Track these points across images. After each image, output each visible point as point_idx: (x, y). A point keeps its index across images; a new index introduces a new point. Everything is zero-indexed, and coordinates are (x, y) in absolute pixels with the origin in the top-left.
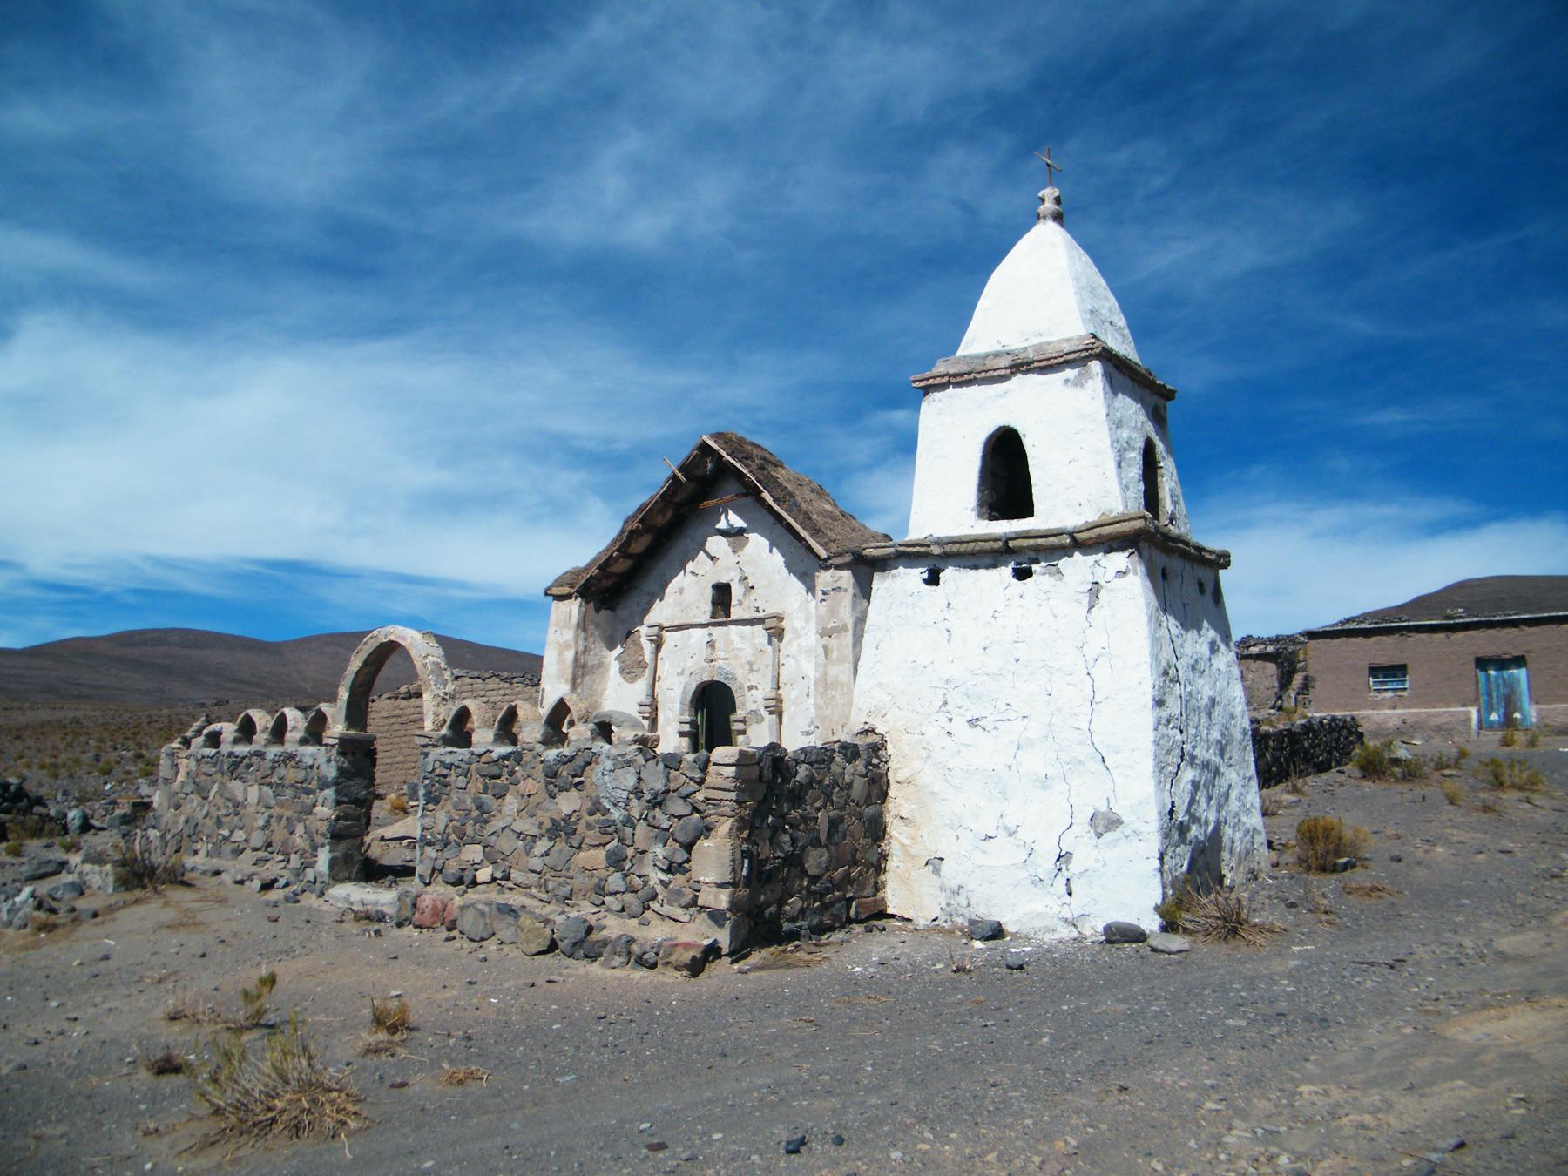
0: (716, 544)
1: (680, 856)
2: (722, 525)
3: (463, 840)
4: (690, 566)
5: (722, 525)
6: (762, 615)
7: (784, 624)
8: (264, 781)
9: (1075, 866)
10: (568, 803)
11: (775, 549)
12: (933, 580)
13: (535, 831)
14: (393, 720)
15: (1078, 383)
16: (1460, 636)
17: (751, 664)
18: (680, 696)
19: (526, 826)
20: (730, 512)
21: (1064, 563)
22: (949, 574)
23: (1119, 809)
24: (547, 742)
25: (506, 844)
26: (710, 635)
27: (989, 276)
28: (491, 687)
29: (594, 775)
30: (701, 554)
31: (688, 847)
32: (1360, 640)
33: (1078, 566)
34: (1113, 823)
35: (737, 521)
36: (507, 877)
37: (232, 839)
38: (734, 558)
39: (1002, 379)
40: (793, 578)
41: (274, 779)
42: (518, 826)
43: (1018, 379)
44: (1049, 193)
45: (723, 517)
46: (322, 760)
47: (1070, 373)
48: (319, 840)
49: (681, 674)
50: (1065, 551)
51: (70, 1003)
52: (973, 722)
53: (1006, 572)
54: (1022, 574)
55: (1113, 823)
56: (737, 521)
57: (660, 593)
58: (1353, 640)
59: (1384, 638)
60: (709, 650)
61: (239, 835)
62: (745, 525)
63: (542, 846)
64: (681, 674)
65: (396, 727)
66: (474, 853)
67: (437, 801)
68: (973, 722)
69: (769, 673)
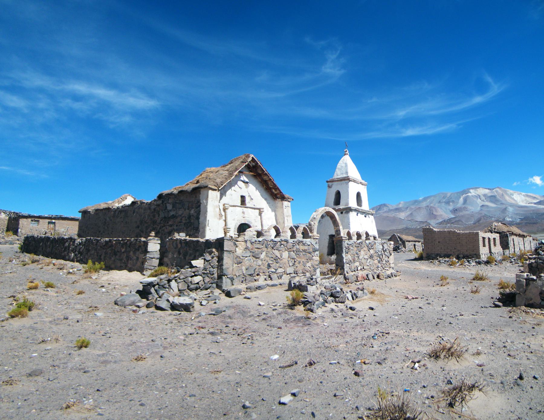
3: (354, 261)
4: (233, 188)
5: (242, 179)
6: (255, 207)
8: (289, 250)
10: (372, 251)
11: (257, 190)
13: (367, 258)
17: (255, 220)
18: (234, 226)
19: (366, 257)
20: (244, 176)
24: (291, 238)
25: (363, 261)
26: (243, 210)
29: (375, 246)
30: (236, 185)
36: (363, 268)
37: (277, 272)
38: (246, 190)
39: (358, 184)
40: (263, 200)
41: (295, 249)
43: (360, 185)
45: (242, 176)
46: (314, 243)
48: (316, 267)
49: (234, 220)
51: (133, 391)
53: (364, 216)
56: (247, 180)
60: (243, 214)
61: (280, 270)
62: (248, 181)
63: (369, 260)
64: (234, 220)
66: (357, 264)
67: (347, 253)
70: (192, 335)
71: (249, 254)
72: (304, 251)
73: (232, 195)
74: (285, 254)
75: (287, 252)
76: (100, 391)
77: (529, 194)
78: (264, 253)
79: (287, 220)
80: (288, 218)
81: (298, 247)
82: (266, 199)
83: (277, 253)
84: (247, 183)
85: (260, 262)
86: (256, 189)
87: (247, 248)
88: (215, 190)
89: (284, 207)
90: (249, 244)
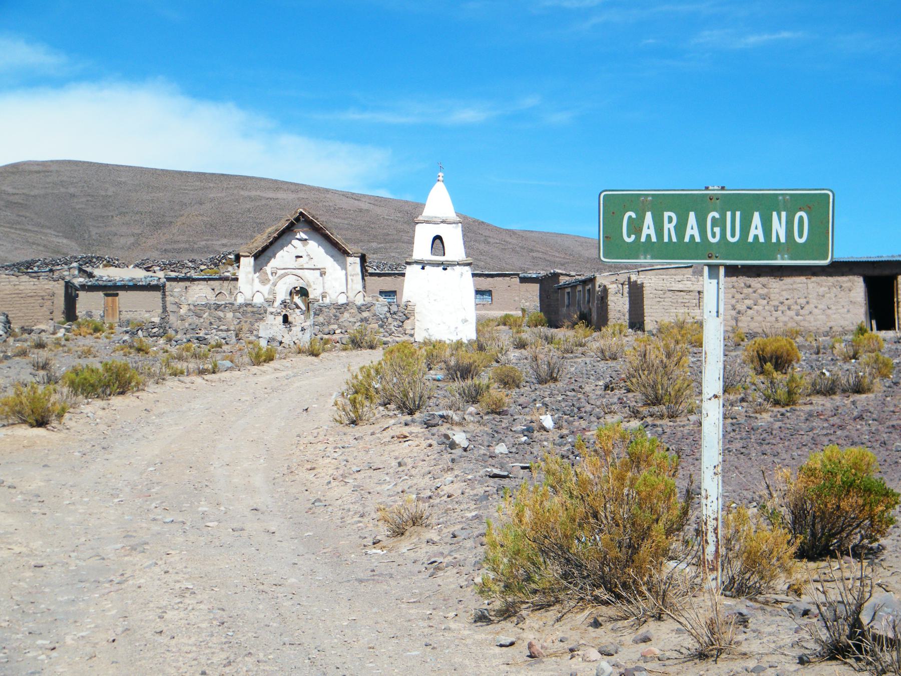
0: (295, 242)
1: (401, 324)
2: (298, 236)
4: (285, 249)
5: (298, 236)
7: (326, 271)
9: (458, 330)
12: (423, 268)
14: (14, 296)
15: (456, 227)
16: (345, 277)
21: (455, 267)
22: (427, 268)
23: (468, 319)
27: (428, 195)
28: (24, 280)
31: (403, 322)
32: (376, 278)
33: (457, 268)
34: (466, 321)
35: (304, 236)
40: (329, 257)
41: (241, 310)
42: (350, 320)
43: (442, 225)
44: (441, 174)
47: (454, 225)
50: (455, 265)
52: (435, 300)
53: (441, 268)
54: (445, 269)
55: (466, 321)
56: (304, 236)
57: (274, 256)
58: (373, 278)
59: (387, 278)
65: (18, 299)
68: (435, 300)
69: (322, 286)
70: (221, 607)
71: (191, 314)
72: (252, 312)
73: (283, 257)
74: (230, 315)
75: (231, 313)
76: (48, 466)
77: (109, 292)
78: (207, 314)
79: (352, 280)
80: (354, 278)
81: (245, 308)
82: (332, 256)
83: (221, 314)
84: (306, 240)
85: (202, 320)
86: (319, 245)
87: (189, 310)
88: (249, 256)
89: (348, 264)
90: (192, 307)
